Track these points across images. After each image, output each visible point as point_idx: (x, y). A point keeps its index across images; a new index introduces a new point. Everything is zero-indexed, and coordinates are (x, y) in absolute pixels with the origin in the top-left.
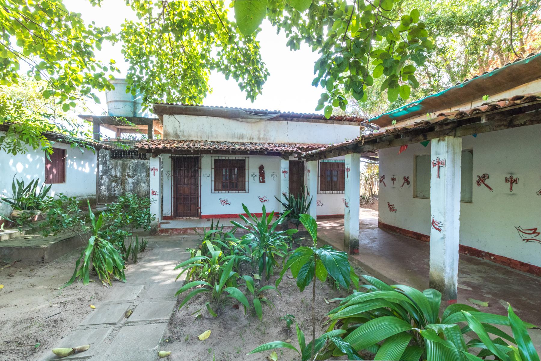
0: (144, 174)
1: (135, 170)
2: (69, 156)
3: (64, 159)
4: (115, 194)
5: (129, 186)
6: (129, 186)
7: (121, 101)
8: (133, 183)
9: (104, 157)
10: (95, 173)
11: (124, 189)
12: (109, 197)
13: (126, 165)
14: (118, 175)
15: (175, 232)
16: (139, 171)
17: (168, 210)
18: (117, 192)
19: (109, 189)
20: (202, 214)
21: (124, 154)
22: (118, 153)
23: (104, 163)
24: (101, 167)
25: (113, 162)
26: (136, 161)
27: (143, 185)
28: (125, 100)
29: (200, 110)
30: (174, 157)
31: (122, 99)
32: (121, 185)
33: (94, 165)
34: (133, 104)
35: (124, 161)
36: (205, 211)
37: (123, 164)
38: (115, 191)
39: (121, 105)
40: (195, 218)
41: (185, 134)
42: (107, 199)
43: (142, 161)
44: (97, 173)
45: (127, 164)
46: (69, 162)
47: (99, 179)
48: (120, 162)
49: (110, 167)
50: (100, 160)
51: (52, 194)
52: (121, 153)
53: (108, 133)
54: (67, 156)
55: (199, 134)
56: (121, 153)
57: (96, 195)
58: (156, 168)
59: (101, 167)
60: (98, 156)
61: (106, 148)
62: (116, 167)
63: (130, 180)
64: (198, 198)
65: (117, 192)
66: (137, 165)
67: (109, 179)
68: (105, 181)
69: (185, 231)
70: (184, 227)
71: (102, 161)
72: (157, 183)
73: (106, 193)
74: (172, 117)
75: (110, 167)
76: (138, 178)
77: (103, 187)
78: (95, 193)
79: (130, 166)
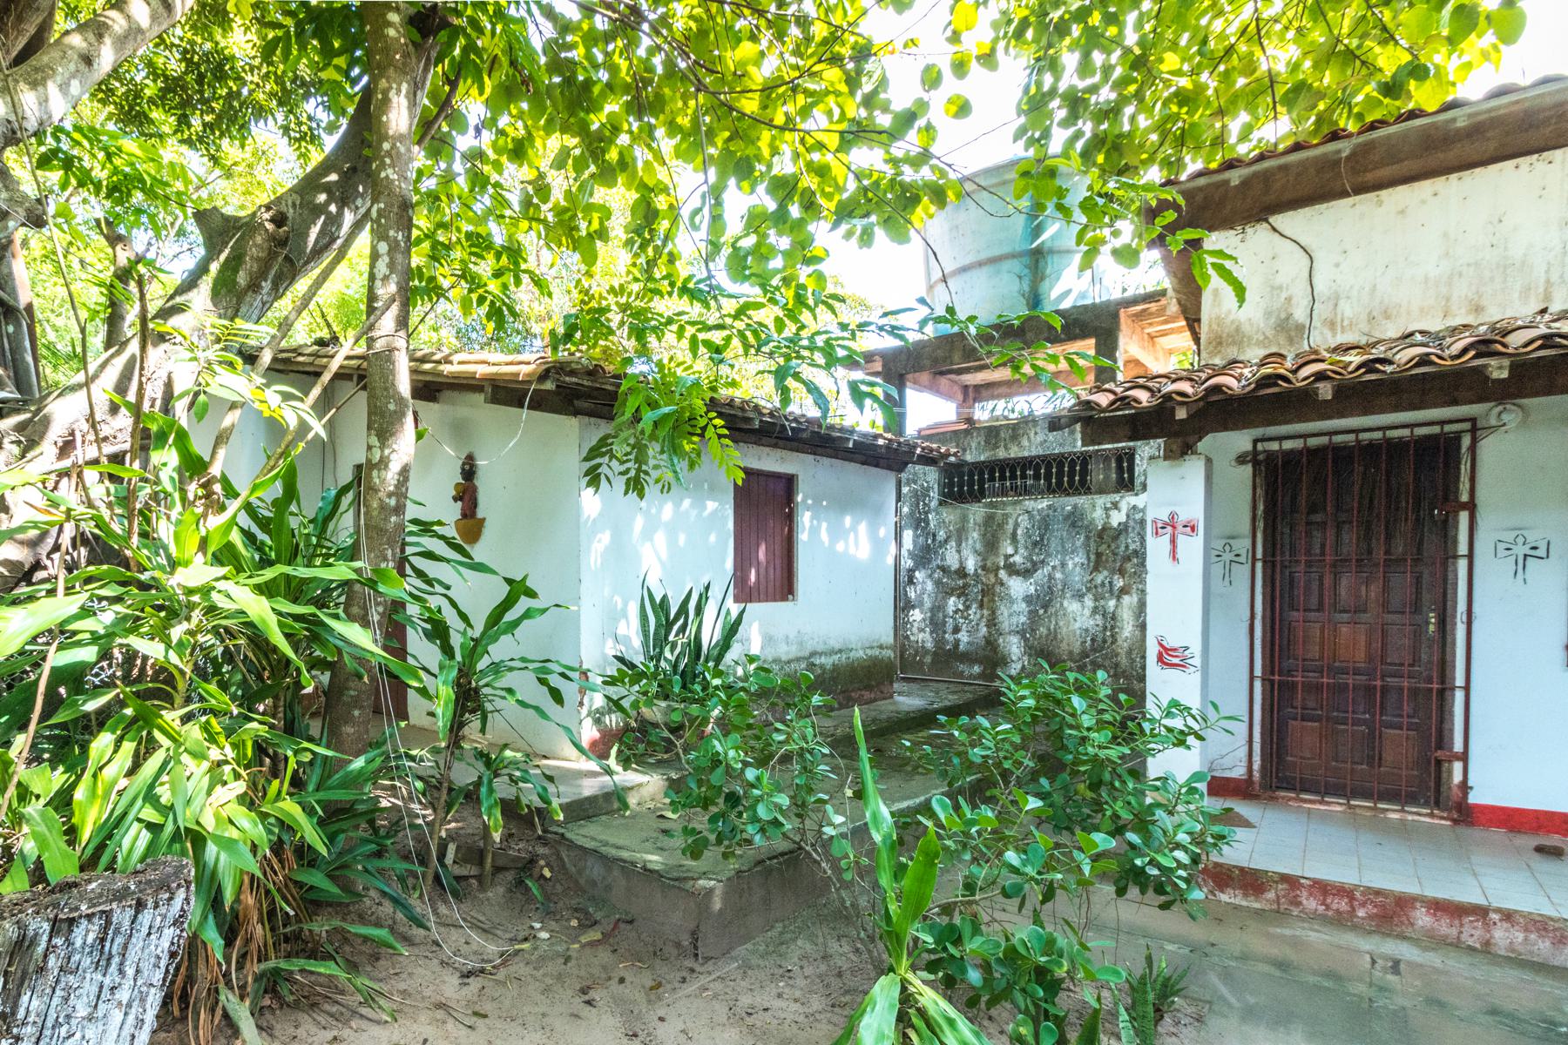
0: (1080, 558)
1: (1038, 545)
2: (804, 500)
3: (791, 510)
4: (957, 642)
5: (1013, 614)
6: (1013, 614)
7: (980, 264)
8: (1028, 599)
9: (920, 496)
10: (890, 561)
11: (992, 623)
12: (935, 654)
13: (1001, 526)
14: (971, 564)
15: (1311, 904)
16: (1054, 544)
17: (1233, 748)
18: (963, 637)
19: (936, 623)
20: (1473, 798)
21: (992, 479)
22: (971, 475)
23: (919, 522)
24: (908, 536)
25: (950, 515)
26: (1043, 504)
27: (1072, 606)
28: (996, 252)
29: (1477, 130)
30: (1270, 455)
31: (984, 256)
32: (981, 606)
33: (886, 531)
34: (1026, 260)
35: (991, 505)
36: (1494, 778)
37: (989, 519)
38: (956, 630)
39: (980, 277)
40: (1418, 816)
41: (1347, 309)
42: (928, 659)
43: (1068, 503)
44: (898, 559)
45: (1006, 516)
46: (805, 519)
47: (903, 580)
48: (976, 512)
49: (942, 535)
50: (906, 510)
51: (752, 639)
52: (981, 474)
53: (928, 410)
54: (799, 498)
55: (1462, 290)
56: (981, 474)
57: (893, 648)
58: (1183, 517)
59: (908, 536)
60: (899, 499)
61: (927, 460)
62: (960, 534)
63: (1018, 587)
64: (1444, 693)
65: (963, 637)
66: (1045, 524)
67: (938, 583)
68: (924, 591)
69: (1391, 912)
70: (1378, 883)
71: (912, 514)
72: (1184, 588)
73: (925, 638)
74: (1258, 235)
75: (942, 535)
76: (1051, 577)
77: (916, 615)
78: (891, 640)
79: (1017, 525)
